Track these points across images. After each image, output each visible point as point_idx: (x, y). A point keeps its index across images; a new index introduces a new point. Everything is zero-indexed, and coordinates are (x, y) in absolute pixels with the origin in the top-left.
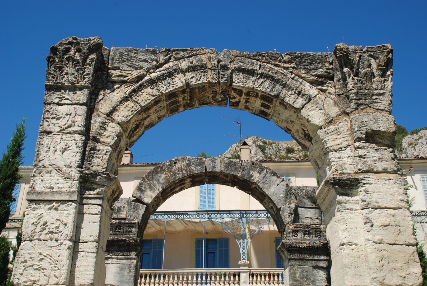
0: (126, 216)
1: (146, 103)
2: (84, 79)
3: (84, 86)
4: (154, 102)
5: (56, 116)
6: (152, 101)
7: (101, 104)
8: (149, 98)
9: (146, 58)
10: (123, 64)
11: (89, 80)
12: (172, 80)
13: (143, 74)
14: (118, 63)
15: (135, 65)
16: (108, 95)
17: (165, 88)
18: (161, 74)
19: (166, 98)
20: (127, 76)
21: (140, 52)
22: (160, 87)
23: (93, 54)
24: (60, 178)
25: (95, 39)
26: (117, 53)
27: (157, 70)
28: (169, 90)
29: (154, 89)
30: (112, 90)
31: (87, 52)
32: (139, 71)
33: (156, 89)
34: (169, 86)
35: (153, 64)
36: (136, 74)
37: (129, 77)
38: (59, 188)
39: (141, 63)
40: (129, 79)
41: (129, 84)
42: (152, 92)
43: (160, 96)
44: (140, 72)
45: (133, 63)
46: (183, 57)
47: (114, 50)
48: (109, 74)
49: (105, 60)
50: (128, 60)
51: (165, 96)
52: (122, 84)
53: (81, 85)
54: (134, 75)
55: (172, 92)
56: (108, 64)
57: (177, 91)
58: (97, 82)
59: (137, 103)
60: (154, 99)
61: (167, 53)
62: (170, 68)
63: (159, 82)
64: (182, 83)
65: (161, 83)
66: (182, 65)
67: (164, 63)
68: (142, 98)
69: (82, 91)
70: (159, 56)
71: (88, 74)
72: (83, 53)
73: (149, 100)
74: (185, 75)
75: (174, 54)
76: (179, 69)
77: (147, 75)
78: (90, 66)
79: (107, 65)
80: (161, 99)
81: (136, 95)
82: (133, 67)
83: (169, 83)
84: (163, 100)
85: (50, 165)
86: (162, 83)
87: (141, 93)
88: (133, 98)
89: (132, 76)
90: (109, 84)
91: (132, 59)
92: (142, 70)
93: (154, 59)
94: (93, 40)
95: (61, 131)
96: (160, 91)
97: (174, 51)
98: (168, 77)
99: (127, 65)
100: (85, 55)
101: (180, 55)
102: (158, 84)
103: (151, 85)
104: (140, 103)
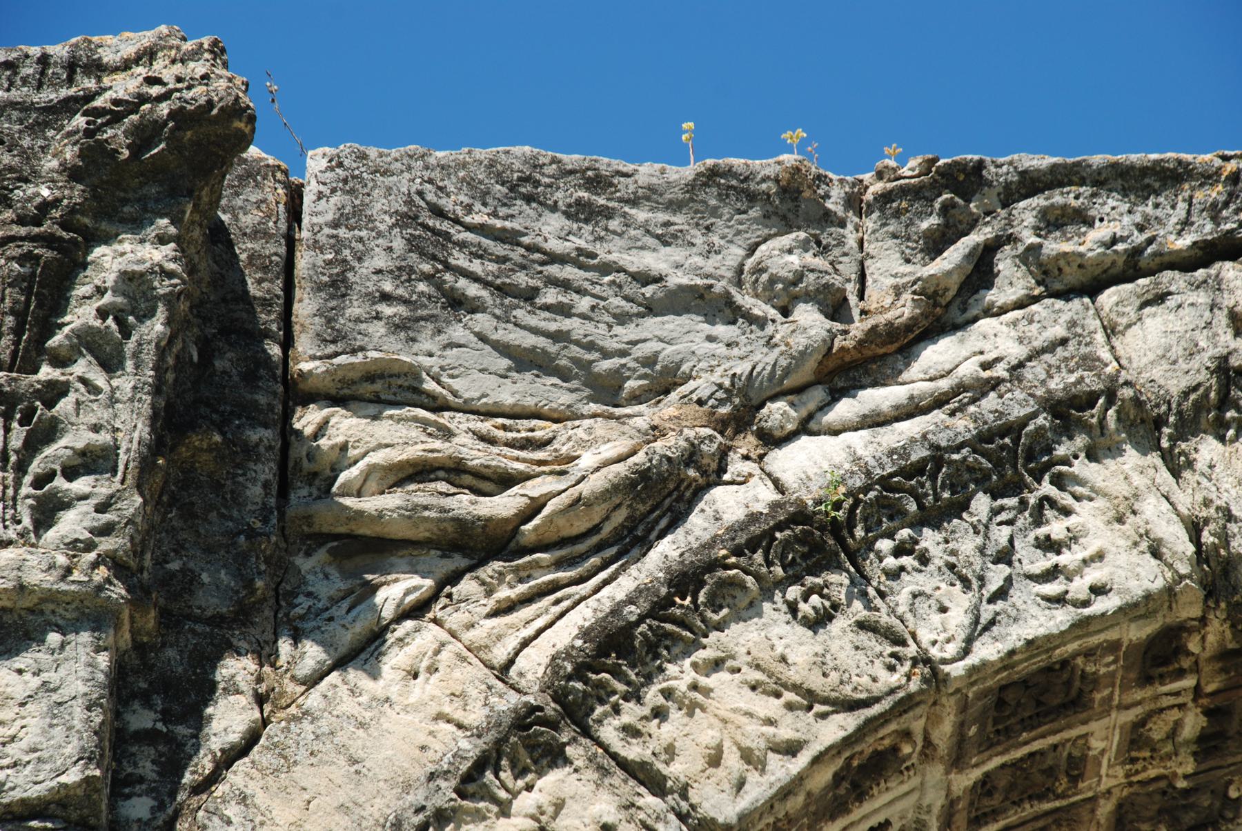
1: (758, 789)
2: (46, 514)
3: (51, 597)
4: (838, 778)
6: (817, 760)
7: (243, 799)
8: (785, 733)
9: (709, 265)
10: (457, 332)
11: (106, 530)
12: (1038, 521)
13: (692, 455)
14: (398, 326)
15: (590, 346)
16: (314, 700)
17: (958, 618)
18: (903, 452)
19: (961, 726)
20: (506, 481)
21: (634, 202)
22: (902, 598)
23: (136, 224)
25: (149, 55)
26: (381, 207)
27: (845, 409)
28: (1015, 635)
29: (840, 624)
30: (347, 638)
31: (72, 210)
32: (644, 415)
33: (862, 625)
34: (1001, 594)
35: (799, 342)
36: (609, 451)
37: (535, 488)
39: (652, 325)
40: (535, 506)
41: (537, 565)
42: (821, 663)
43: (906, 705)
44: (657, 431)
45: (566, 324)
46: (1137, 251)
47: (349, 183)
48: (298, 451)
49: (253, 289)
50: (502, 290)
51: (964, 707)
52: (459, 562)
53: (21, 588)
54: (587, 460)
55: (1040, 661)
56: (287, 343)
57: (1089, 653)
58: (179, 548)
59: (657, 785)
60: (847, 742)
61: (946, 209)
62: (994, 384)
63: (885, 545)
64: (1156, 553)
65: (907, 561)
66: (1130, 344)
67: (914, 321)
68: (705, 732)
69: (24, 660)
70: (851, 241)
72: (21, 221)
73: (791, 749)
74: (1177, 466)
75: (1030, 219)
76: (1111, 396)
77: (736, 466)
78: (110, 364)
79: (275, 350)
80: (907, 735)
81: (635, 696)
82: (565, 376)
83: (1005, 556)
84: (928, 742)
86: (924, 559)
87: (690, 676)
88: (609, 732)
89: (576, 470)
90: (304, 564)
91: (553, 282)
92: (670, 407)
93: (799, 277)
94: (126, 65)
96: (911, 650)
97: (1030, 184)
98: (983, 481)
99: (503, 349)
100: (48, 240)
101: (1101, 232)
102: (872, 567)
103: (796, 579)
104: (684, 793)
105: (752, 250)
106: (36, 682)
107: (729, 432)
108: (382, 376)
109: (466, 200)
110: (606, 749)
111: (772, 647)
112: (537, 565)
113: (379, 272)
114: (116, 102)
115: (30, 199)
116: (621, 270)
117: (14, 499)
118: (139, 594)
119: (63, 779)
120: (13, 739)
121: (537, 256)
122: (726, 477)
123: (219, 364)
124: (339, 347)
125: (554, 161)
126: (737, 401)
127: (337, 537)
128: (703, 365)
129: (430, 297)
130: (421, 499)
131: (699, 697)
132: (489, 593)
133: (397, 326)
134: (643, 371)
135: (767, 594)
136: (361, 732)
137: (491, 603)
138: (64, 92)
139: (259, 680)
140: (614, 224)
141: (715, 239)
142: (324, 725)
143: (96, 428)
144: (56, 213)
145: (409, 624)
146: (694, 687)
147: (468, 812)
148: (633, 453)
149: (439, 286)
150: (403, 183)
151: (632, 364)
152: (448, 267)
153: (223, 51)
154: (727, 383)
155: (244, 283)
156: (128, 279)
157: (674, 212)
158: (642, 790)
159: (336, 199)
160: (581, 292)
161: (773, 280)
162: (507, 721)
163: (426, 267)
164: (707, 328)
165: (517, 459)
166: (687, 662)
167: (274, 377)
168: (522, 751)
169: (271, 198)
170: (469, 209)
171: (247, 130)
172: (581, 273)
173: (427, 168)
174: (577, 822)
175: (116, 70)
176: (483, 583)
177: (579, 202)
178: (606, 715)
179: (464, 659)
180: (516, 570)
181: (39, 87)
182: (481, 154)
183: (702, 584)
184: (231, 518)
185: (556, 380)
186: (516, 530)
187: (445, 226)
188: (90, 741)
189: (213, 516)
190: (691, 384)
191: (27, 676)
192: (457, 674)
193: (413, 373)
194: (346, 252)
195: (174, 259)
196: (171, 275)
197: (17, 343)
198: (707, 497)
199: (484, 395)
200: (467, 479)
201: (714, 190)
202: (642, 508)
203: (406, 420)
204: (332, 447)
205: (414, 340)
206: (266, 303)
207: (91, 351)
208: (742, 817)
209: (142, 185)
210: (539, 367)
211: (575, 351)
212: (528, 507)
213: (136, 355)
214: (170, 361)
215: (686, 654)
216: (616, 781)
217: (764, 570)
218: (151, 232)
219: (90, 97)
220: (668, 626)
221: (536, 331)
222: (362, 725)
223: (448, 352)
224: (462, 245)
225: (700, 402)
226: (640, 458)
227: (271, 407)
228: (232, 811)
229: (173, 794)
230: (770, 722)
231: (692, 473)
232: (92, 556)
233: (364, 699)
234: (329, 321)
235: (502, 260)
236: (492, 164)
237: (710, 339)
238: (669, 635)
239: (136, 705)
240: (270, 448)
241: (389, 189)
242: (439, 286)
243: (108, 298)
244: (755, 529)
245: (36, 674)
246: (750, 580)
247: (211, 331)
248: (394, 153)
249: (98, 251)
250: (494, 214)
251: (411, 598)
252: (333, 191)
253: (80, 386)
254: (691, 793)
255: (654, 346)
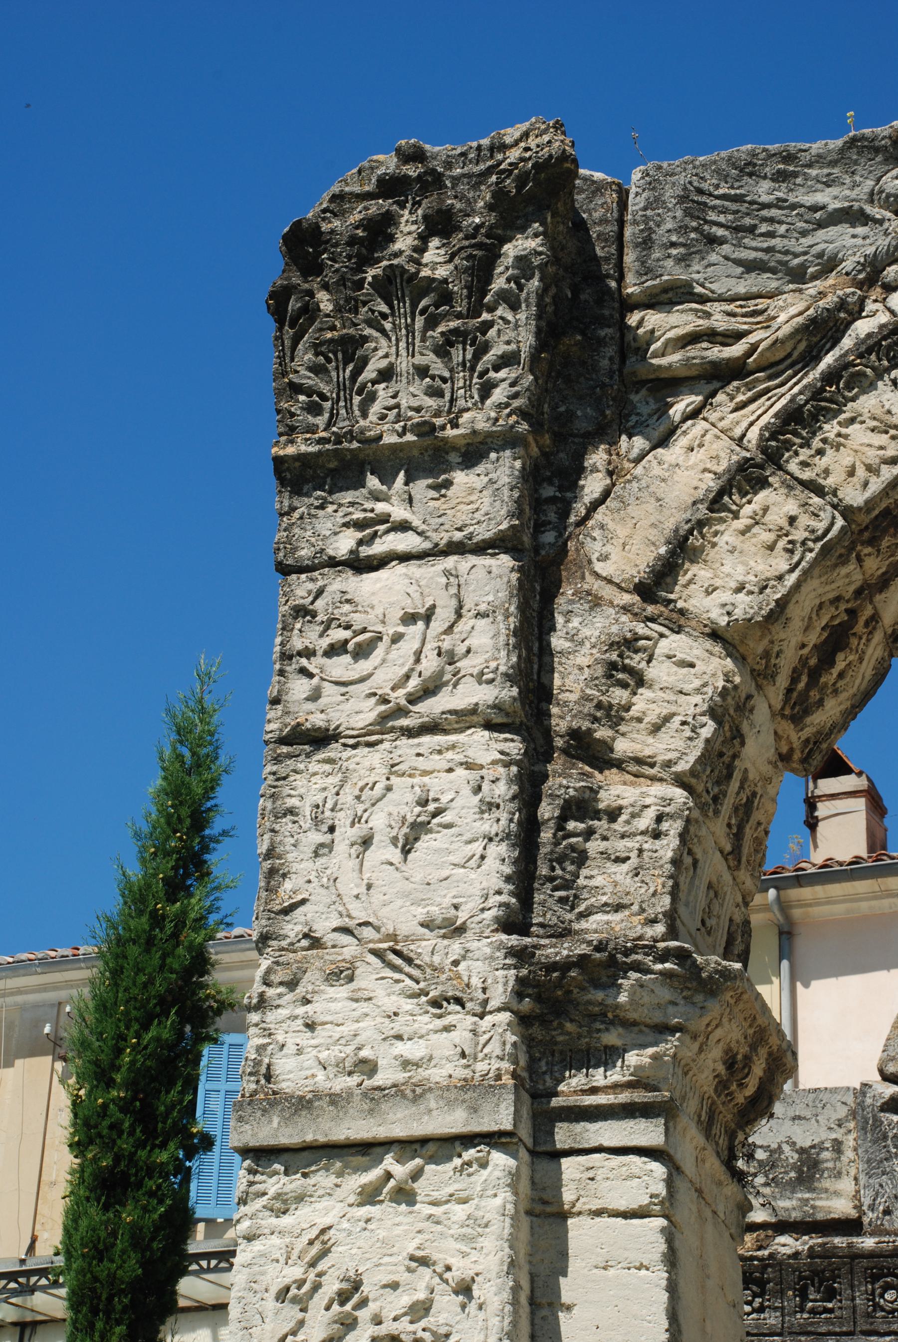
0: (858, 1207)
1: (876, 485)
2: (486, 390)
3: (490, 434)
5: (347, 634)
7: (602, 527)
9: (853, 194)
10: (713, 257)
11: (515, 396)
13: (842, 304)
15: (787, 252)
16: (639, 470)
20: (739, 336)
21: (810, 165)
23: (523, 229)
24: (408, 1005)
25: (526, 135)
26: (670, 194)
30: (656, 435)
31: (491, 227)
32: (812, 289)
37: (752, 338)
38: (406, 1064)
39: (821, 234)
40: (754, 348)
41: (757, 380)
44: (822, 294)
45: (773, 242)
48: (629, 337)
49: (599, 252)
50: (737, 229)
52: (716, 384)
53: (474, 432)
54: (783, 317)
56: (621, 279)
59: (820, 491)
68: (846, 458)
69: (480, 469)
71: (507, 360)
72: (467, 238)
77: (870, 306)
78: (514, 307)
79: (613, 284)
81: (807, 444)
82: (774, 271)
85: (345, 930)
89: (775, 325)
90: (635, 398)
91: (764, 220)
94: (516, 143)
95: (384, 718)
99: (738, 262)
100: (480, 246)
104: (835, 493)
105: (878, 180)
106: (486, 479)
107: (865, 288)
108: (672, 289)
109: (715, 181)
110: (791, 475)
111: (883, 406)
112: (757, 380)
113: (669, 231)
114: (510, 164)
115: (470, 225)
116: (802, 206)
117: (470, 386)
118: (537, 426)
119: (501, 527)
120: (477, 510)
121: (755, 206)
122: (864, 314)
123: (583, 297)
124: (649, 276)
125: (764, 150)
126: (868, 269)
127: (651, 381)
128: (850, 252)
129: (697, 240)
130: (691, 354)
131: (842, 440)
132: (732, 399)
133: (680, 260)
134: (817, 261)
135: (880, 377)
136: (663, 484)
137: (732, 405)
138: (489, 163)
139: (609, 463)
140: (799, 180)
141: (857, 178)
142: (643, 483)
143: (508, 343)
144: (483, 231)
145: (690, 422)
146: (839, 435)
147: (715, 519)
148: (808, 309)
149: (702, 233)
150: (682, 179)
151: (811, 259)
152: (706, 222)
153: (562, 125)
154: (862, 260)
155: (594, 249)
156: (519, 259)
157: (833, 167)
158: (812, 495)
159: (645, 195)
160: (780, 222)
161: (888, 196)
162: (734, 468)
163: (694, 224)
164: (852, 231)
165: (745, 323)
166: (835, 421)
167: (613, 299)
168: (744, 483)
169: (609, 201)
170: (717, 187)
171: (573, 167)
172: (780, 212)
173: (694, 167)
174: (776, 517)
175: (512, 146)
176: (728, 395)
177: (779, 171)
178: (790, 457)
179: (718, 437)
180: (746, 385)
181: (477, 164)
182: (724, 154)
183: (842, 377)
184: (592, 379)
185: (769, 275)
186: (745, 363)
187: (704, 199)
188: (512, 506)
189: (582, 379)
190: (844, 264)
191: (482, 477)
192: (715, 446)
193: (688, 285)
194: (651, 223)
195: (542, 245)
196: (540, 254)
197: (469, 303)
198: (853, 327)
199: (729, 290)
200: (719, 339)
201: (855, 150)
202: (815, 339)
203: (686, 311)
204: (645, 333)
205: (689, 266)
206: (607, 259)
207: (505, 302)
208: (867, 502)
209: (525, 207)
210: (760, 269)
211: (779, 256)
212: (749, 349)
213: (526, 300)
214: (548, 300)
215: (835, 417)
216: (797, 492)
217: (877, 364)
218: (530, 231)
219: (500, 163)
220: (823, 404)
221: (756, 249)
222: (663, 480)
223: (709, 269)
224: (713, 208)
225: (847, 274)
226: (811, 312)
227: (612, 316)
228: (596, 533)
229: (565, 528)
230: (881, 448)
231: (842, 315)
232: (508, 410)
233: (665, 466)
234: (643, 263)
235: (736, 212)
236: (730, 158)
237: (854, 236)
238: (825, 408)
239: (545, 485)
240: (612, 338)
241: (674, 184)
242: (702, 233)
243: (510, 272)
244: (870, 342)
245: (486, 475)
246: (868, 371)
247: (578, 279)
248: (677, 163)
249: (506, 247)
250: (732, 187)
251: (688, 409)
252: (644, 190)
253: (500, 321)
254: (839, 493)
255: (822, 246)
